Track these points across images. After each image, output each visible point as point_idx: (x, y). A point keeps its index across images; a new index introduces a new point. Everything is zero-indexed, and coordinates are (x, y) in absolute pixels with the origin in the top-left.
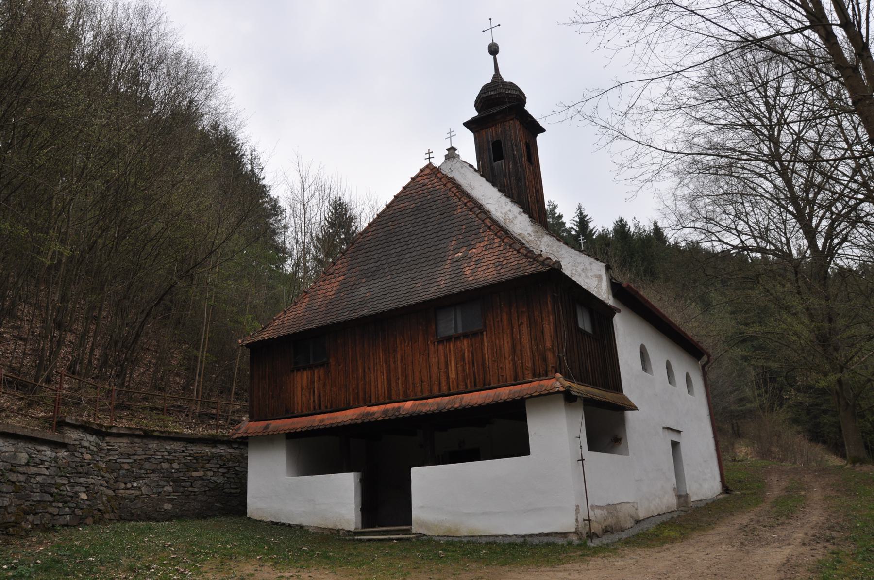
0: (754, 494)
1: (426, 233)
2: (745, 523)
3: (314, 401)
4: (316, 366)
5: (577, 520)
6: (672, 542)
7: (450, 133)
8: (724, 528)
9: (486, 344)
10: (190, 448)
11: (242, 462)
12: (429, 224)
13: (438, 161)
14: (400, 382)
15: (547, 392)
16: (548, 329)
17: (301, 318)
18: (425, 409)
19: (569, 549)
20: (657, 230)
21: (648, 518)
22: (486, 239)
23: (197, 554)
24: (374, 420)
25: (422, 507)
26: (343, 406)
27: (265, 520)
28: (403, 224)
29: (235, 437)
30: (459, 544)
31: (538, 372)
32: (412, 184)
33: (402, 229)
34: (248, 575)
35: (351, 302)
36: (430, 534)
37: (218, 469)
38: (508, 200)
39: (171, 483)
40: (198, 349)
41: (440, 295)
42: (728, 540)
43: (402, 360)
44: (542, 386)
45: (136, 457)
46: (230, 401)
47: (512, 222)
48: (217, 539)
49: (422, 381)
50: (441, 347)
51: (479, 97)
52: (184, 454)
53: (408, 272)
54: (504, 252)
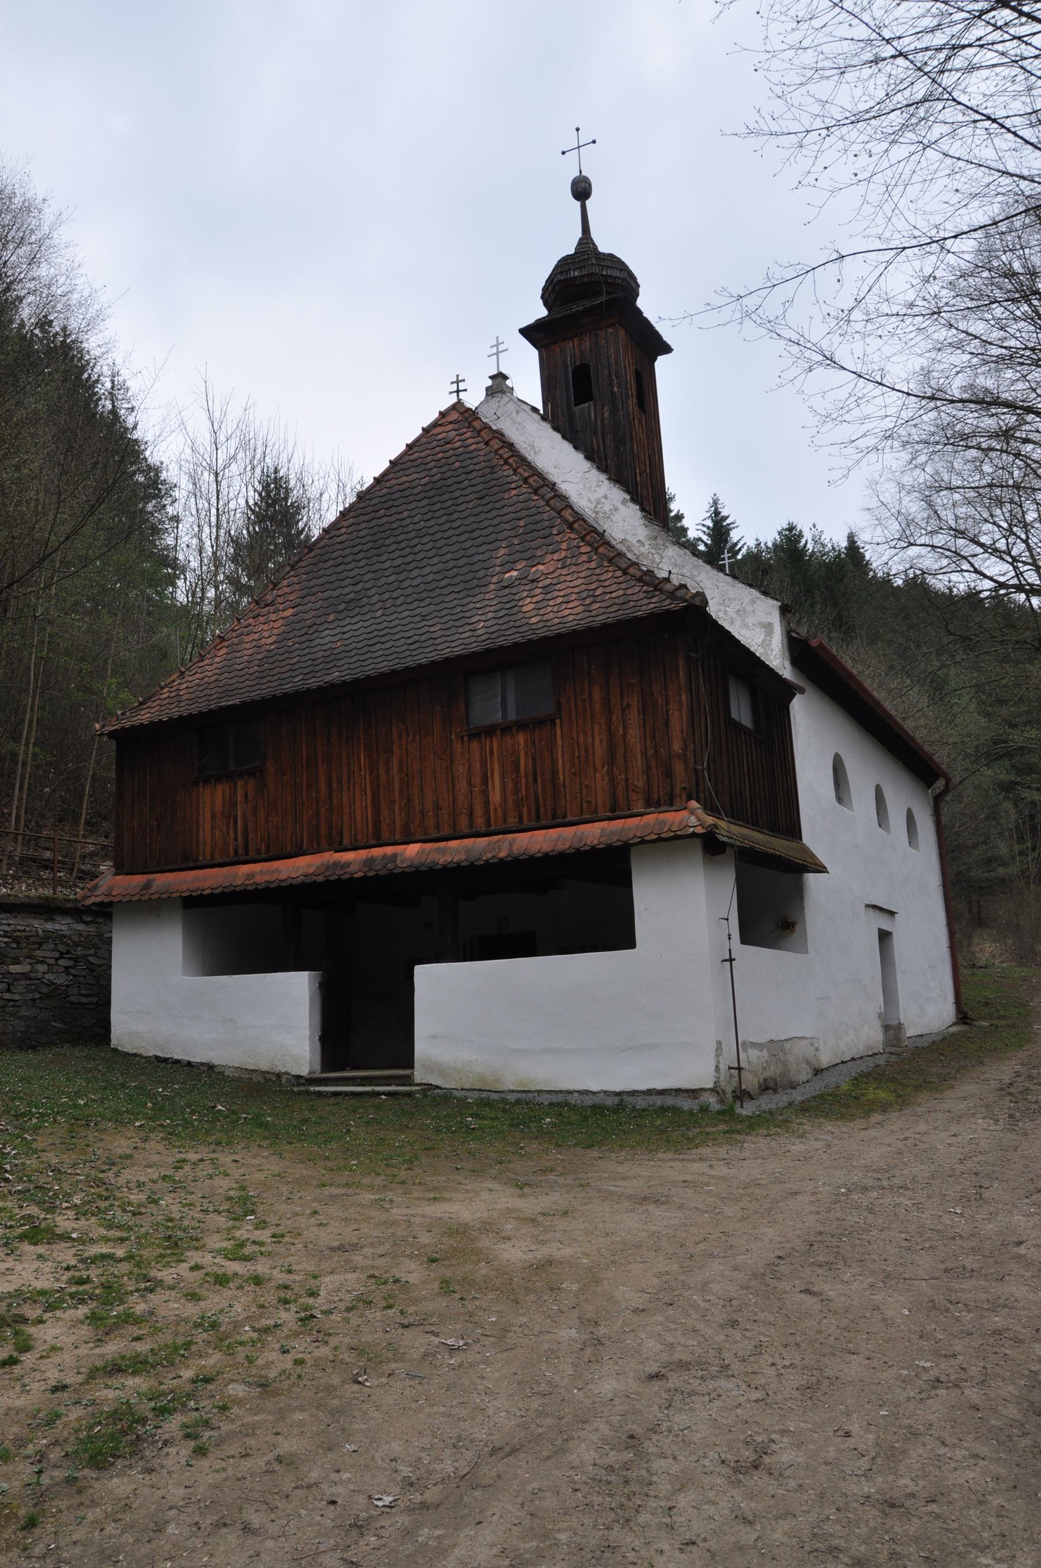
0: (1013, 1026)
1: (451, 532)
2: (1007, 1078)
3: (236, 839)
5: (717, 1067)
6: (885, 1111)
7: (497, 345)
8: (971, 1088)
9: (559, 743)
10: (5, 922)
11: (100, 948)
12: (455, 516)
13: (474, 398)
14: (397, 807)
15: (672, 834)
16: (678, 720)
17: (212, 685)
18: (443, 859)
19: (702, 1118)
20: (853, 548)
21: (834, 1066)
22: (564, 546)
23: (23, 1115)
24: (346, 876)
25: (434, 1037)
26: (289, 849)
27: (145, 1054)
28: (406, 514)
29: (89, 902)
30: (501, 1106)
31: (656, 796)
32: (424, 440)
33: (404, 523)
34: (120, 1157)
35: (308, 657)
36: (447, 1086)
37: (57, 959)
38: (603, 477)
40: (17, 739)
41: (475, 647)
42: (983, 1110)
43: (400, 766)
44: (663, 823)
46: (77, 836)
47: (609, 518)
48: (59, 1087)
49: (437, 808)
50: (475, 745)
51: (550, 281)
53: (416, 604)
54: (598, 571)
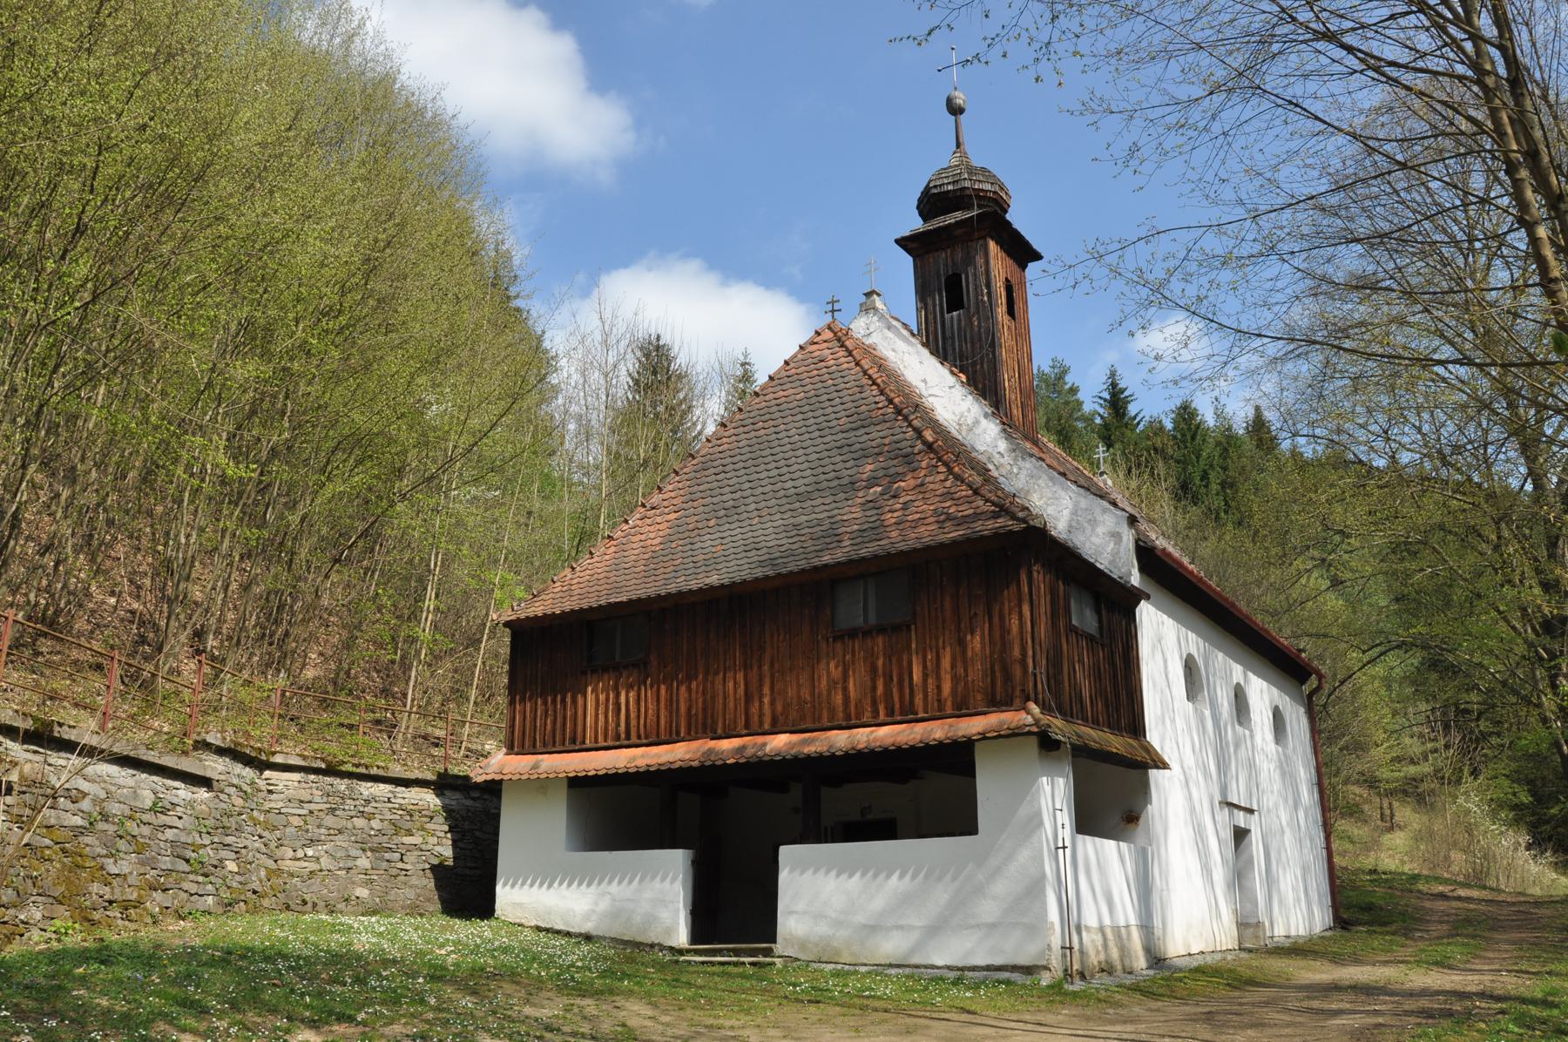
4: (626, 667)
18: (809, 749)
39: (369, 854)
45: (312, 806)
50: (839, 645)
52: (391, 805)
